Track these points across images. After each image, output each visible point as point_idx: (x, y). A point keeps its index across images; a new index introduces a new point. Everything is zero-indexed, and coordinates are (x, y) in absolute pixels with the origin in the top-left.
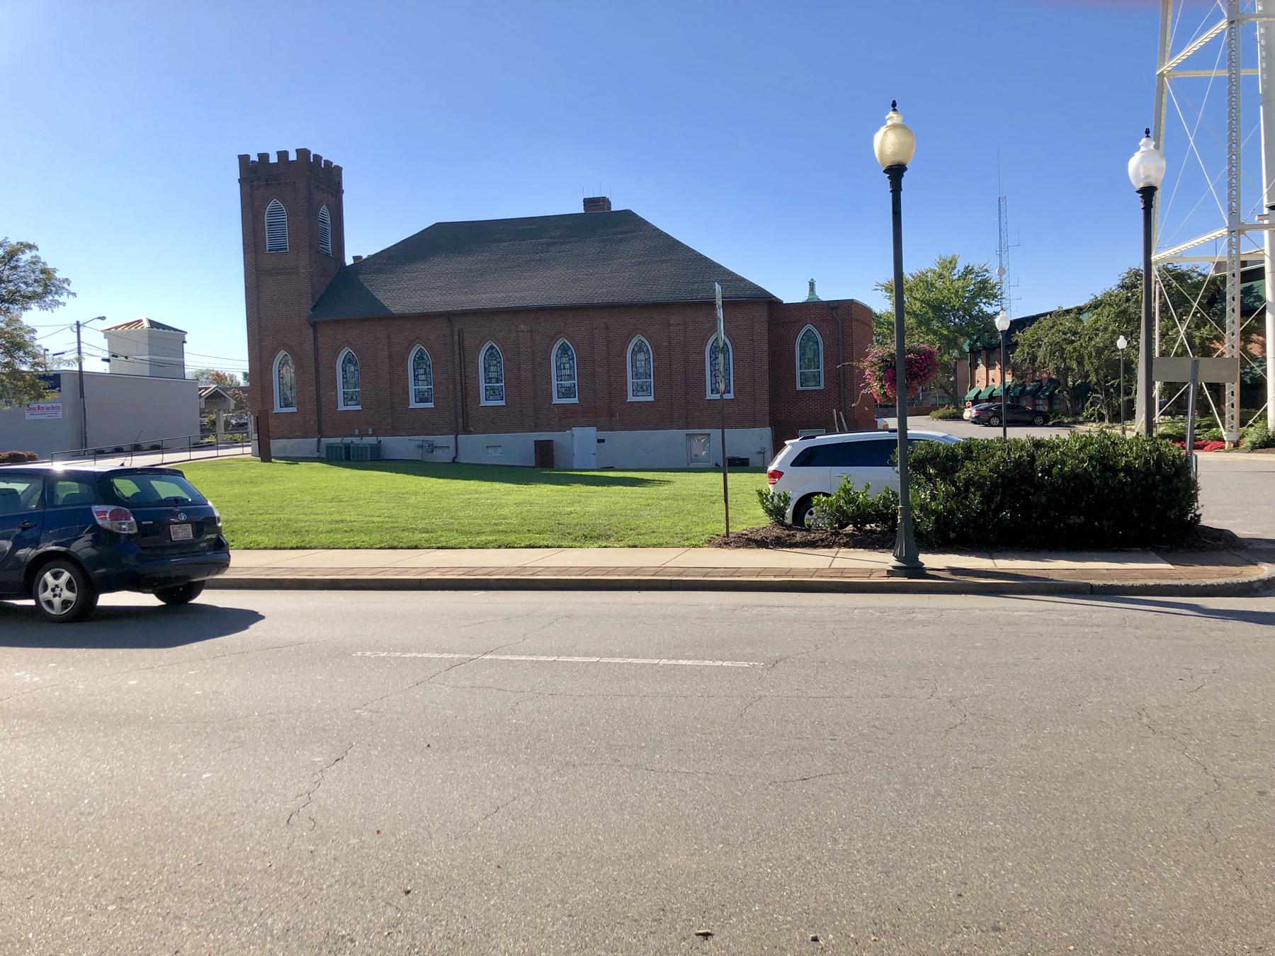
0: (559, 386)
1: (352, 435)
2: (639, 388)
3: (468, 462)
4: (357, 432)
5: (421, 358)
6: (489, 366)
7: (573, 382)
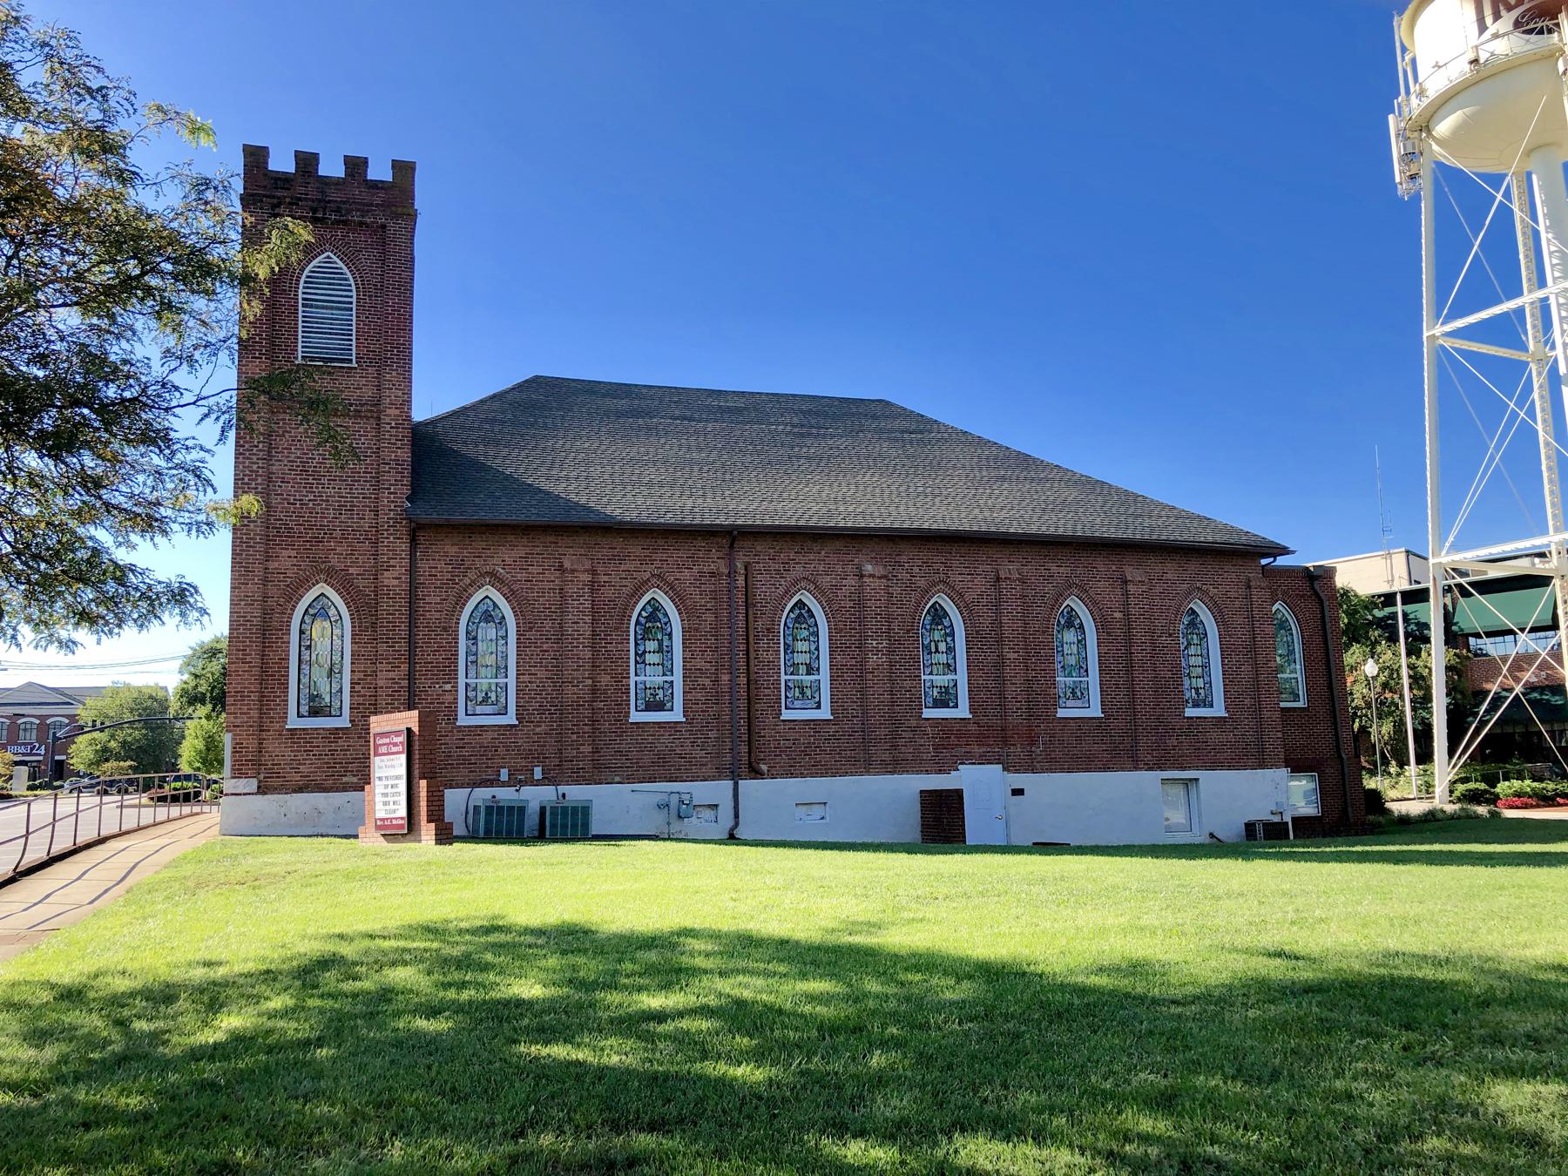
0: (928, 684)
3: (694, 845)
5: (652, 617)
6: (795, 639)
7: (637, 678)
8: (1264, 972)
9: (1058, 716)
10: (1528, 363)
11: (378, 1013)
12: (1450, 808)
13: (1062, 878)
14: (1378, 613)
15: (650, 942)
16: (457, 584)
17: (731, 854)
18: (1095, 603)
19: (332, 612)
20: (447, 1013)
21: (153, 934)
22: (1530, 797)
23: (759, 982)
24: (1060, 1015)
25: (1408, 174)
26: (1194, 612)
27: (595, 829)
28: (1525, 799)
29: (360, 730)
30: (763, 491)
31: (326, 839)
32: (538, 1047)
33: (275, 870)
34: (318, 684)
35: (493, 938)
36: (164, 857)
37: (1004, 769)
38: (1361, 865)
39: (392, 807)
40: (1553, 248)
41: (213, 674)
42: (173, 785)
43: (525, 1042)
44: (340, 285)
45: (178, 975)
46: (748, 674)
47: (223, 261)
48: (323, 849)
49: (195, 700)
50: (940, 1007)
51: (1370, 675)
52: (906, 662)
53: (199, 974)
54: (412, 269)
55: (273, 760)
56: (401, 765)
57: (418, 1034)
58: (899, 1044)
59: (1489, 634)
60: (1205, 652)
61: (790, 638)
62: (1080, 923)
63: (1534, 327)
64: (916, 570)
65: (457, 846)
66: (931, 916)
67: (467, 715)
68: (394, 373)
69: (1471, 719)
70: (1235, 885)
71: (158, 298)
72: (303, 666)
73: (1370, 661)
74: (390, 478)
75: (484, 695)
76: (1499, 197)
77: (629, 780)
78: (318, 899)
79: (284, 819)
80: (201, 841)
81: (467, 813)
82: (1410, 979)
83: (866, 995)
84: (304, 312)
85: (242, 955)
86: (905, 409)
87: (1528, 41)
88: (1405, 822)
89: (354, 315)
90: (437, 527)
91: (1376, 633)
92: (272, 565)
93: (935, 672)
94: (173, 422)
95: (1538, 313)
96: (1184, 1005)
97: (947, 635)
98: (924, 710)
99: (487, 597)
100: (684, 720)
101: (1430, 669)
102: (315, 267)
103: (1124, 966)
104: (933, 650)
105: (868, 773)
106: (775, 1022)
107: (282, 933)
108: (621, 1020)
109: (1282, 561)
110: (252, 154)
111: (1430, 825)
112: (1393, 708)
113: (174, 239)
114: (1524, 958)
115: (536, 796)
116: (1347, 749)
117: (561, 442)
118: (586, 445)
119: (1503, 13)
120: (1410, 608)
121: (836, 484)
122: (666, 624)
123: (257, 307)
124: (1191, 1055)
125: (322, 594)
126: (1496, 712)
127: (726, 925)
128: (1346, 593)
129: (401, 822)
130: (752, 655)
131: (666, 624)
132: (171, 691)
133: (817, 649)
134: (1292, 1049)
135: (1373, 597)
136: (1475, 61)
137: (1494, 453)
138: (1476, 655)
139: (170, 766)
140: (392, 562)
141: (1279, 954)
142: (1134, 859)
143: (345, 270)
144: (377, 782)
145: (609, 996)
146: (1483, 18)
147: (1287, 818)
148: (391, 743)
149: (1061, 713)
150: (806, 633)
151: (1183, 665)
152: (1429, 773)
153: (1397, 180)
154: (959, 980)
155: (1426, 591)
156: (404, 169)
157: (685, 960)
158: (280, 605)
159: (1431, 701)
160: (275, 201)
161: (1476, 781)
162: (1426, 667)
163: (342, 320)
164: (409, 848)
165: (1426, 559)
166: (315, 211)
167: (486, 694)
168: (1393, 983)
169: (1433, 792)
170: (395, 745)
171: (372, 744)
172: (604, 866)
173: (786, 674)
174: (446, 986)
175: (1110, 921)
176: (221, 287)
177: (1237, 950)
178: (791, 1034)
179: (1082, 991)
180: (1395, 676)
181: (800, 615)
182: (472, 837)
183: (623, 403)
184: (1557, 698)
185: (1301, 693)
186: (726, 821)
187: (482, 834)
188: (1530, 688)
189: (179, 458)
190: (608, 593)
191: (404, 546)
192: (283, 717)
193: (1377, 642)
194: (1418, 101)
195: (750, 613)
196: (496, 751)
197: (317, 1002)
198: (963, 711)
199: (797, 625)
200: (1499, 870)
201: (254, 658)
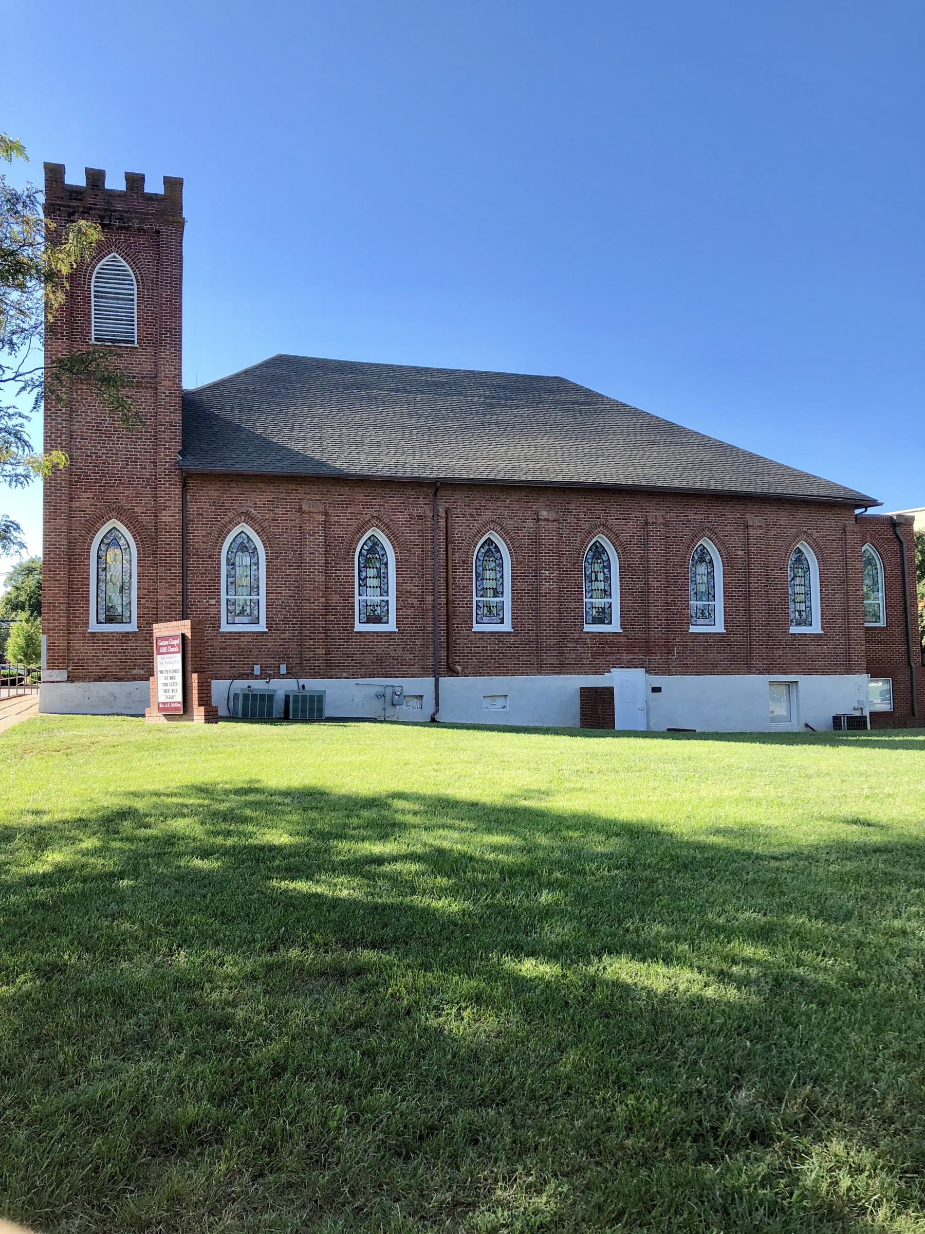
0: (589, 606)
1: (250, 676)
3: (405, 727)
4: (257, 670)
5: (372, 550)
7: (361, 598)
8: (843, 836)
9: (690, 631)
15: (372, 803)
16: (219, 521)
19: (122, 542)
20: (217, 855)
23: (455, 835)
24: (685, 866)
26: (800, 551)
27: (328, 713)
29: (145, 633)
31: (120, 717)
32: (287, 882)
33: (82, 741)
35: (251, 797)
37: (646, 672)
39: (171, 694)
43: (277, 879)
45: (13, 821)
46: (447, 595)
50: (593, 857)
56: (178, 662)
57: (196, 871)
58: (561, 885)
62: (703, 793)
64: (582, 515)
65: (221, 724)
66: (588, 786)
67: (228, 623)
74: (166, 436)
75: (241, 608)
77: (354, 676)
80: (25, 717)
83: (537, 847)
84: (95, 301)
85: (60, 806)
86: (577, 385)
89: (136, 304)
92: (75, 504)
93: (594, 596)
96: (780, 860)
97: (604, 567)
98: (585, 625)
100: (397, 630)
106: (467, 867)
107: (89, 790)
109: (871, 511)
115: (282, 687)
121: (519, 445)
122: (383, 555)
124: (785, 899)
125: (114, 528)
127: (429, 790)
130: (451, 581)
131: (383, 555)
133: (502, 577)
140: (168, 504)
141: (856, 822)
143: (128, 267)
144: (159, 675)
147: (866, 713)
148: (169, 645)
149: (693, 629)
151: (790, 592)
156: (174, 185)
157: (400, 817)
160: (71, 210)
170: (173, 646)
171: (155, 645)
174: (215, 834)
175: (726, 793)
179: (702, 847)
181: (489, 550)
182: (232, 718)
185: (881, 615)
186: (429, 709)
187: (240, 715)
190: (338, 530)
191: (178, 491)
196: (251, 651)
198: (615, 627)
199: (486, 558)
201: (62, 575)
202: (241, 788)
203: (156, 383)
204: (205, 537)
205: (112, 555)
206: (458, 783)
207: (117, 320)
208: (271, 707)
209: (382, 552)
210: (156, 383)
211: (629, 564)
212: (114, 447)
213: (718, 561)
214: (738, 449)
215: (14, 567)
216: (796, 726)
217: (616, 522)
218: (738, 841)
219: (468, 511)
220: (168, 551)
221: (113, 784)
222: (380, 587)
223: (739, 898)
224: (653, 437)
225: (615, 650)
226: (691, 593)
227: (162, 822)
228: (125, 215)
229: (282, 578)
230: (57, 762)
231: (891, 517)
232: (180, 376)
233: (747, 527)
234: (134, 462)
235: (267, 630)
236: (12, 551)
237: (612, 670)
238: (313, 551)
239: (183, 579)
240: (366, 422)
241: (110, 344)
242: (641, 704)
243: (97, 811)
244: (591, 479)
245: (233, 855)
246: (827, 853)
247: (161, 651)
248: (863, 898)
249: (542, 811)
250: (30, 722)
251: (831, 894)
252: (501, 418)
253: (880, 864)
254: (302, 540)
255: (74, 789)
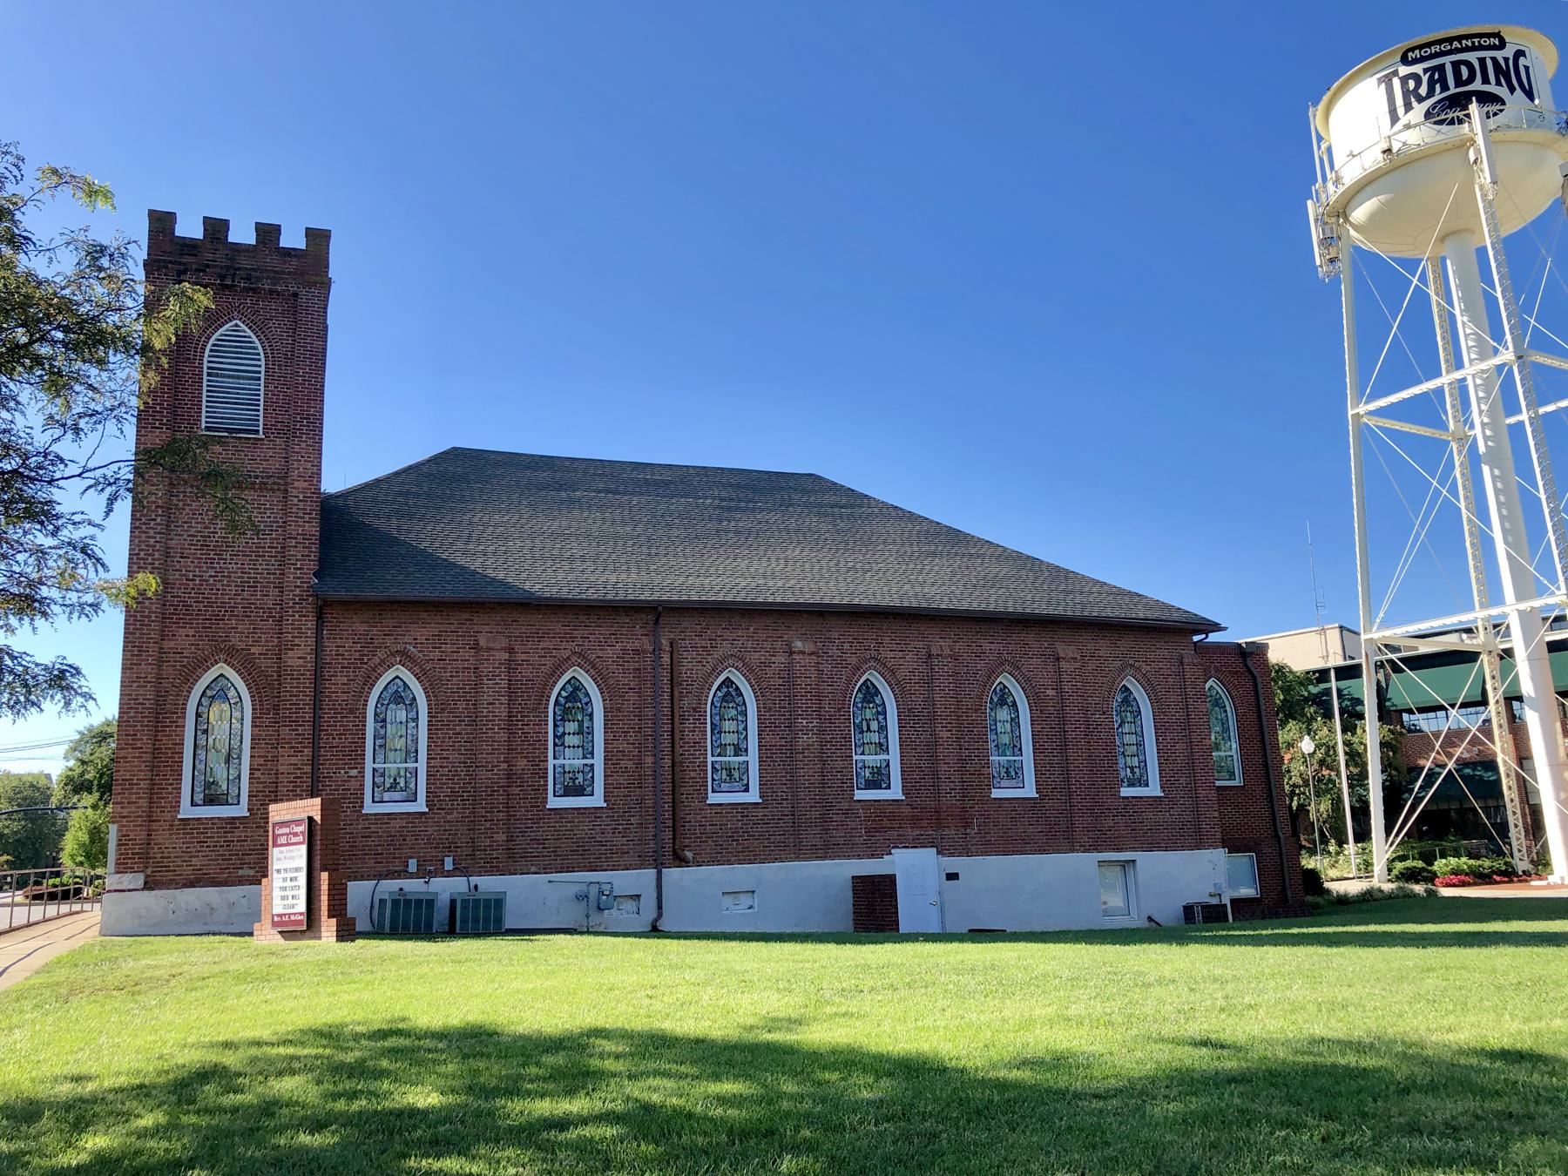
0: (860, 765)
1: (403, 873)
2: (1003, 774)
4: (413, 865)
5: (572, 697)
7: (556, 762)
8: (1188, 1062)
9: (992, 796)
10: (1449, 442)
11: (258, 1130)
12: (1388, 887)
13: (993, 967)
14: (1314, 690)
15: (556, 1044)
16: (366, 663)
17: (651, 948)
18: (1028, 680)
19: (232, 693)
20: (334, 1127)
21: (18, 1046)
22: (1467, 874)
23: (670, 1084)
24: (978, 1112)
25: (1328, 257)
26: (1127, 689)
27: (509, 923)
28: (1462, 877)
29: (258, 820)
30: (690, 566)
31: (218, 938)
32: (430, 1161)
33: (158, 973)
34: (215, 769)
35: (391, 1042)
36: (37, 961)
38: (1295, 948)
39: (290, 901)
40: (1468, 331)
41: (102, 760)
42: (51, 882)
43: (416, 1156)
44: (248, 354)
45: (42, 1092)
46: (673, 756)
47: (118, 328)
48: (214, 948)
49: (81, 789)
50: (856, 1107)
51: (1306, 752)
52: (836, 746)
53: (65, 1090)
54: (324, 338)
55: (163, 853)
56: (301, 856)
57: (305, 1150)
58: (811, 1147)
59: (1422, 710)
60: (1139, 729)
61: (718, 718)
62: (1007, 1013)
63: (1453, 406)
64: (847, 646)
65: (360, 942)
66: (855, 1010)
67: (373, 802)
68: (303, 445)
69: (1406, 795)
70: (1167, 971)
71: (47, 366)
72: (199, 752)
73: (1307, 738)
74: (295, 553)
75: (392, 781)
76: (1415, 281)
77: (546, 870)
78: (204, 1004)
79: (172, 917)
80: (77, 943)
81: (372, 907)
82: (1334, 1066)
83: (781, 1096)
84: (208, 381)
85: (114, 1068)
86: (836, 484)
87: (1438, 131)
88: (1343, 901)
89: (262, 385)
90: (345, 604)
91: (1312, 710)
92: (168, 645)
93: (867, 752)
94: (57, 495)
95: (1456, 392)
96: (1105, 1098)
97: (878, 713)
98: (856, 792)
99: (397, 677)
100: (605, 805)
101: (1365, 745)
102: (221, 335)
103: (1048, 1059)
104: (865, 729)
105: (798, 858)
106: (683, 1127)
107: (160, 1044)
108: (521, 1129)
109: (1214, 637)
110: (159, 220)
111: (1368, 905)
112: (1331, 786)
113: (67, 306)
114: (1447, 1043)
115: (447, 887)
116: (1284, 829)
117: (479, 516)
118: (507, 518)
119: (1415, 104)
120: (1344, 684)
121: (765, 558)
122: (586, 704)
123: (153, 378)
124: (1109, 1152)
125: (222, 675)
126: (1431, 787)
127: (639, 1024)
128: (1281, 670)
129: (300, 918)
130: (677, 737)
131: (586, 704)
132: (54, 778)
133: (746, 729)
134: (1211, 1143)
135: (1308, 673)
136: (1388, 151)
137: (1419, 531)
138: (1409, 731)
139: (51, 860)
140: (297, 641)
141: (1205, 1043)
142: (1068, 946)
143: (254, 338)
144: (275, 875)
145: (509, 1103)
146: (1396, 109)
147: (1226, 901)
148: (290, 833)
149: (996, 793)
150: (734, 712)
151: (1118, 743)
152: (1367, 851)
153: (1318, 263)
154: (878, 1078)
155: (1359, 666)
156: (319, 238)
157: (595, 1063)
158: (176, 687)
159: (1367, 778)
160: (182, 268)
161: (1414, 859)
162: (1361, 743)
163: (250, 389)
164: (308, 947)
165: (1357, 634)
166: (223, 278)
167: (395, 779)
168: (1317, 1070)
169: (1373, 871)
170: (295, 834)
171: (270, 833)
172: (515, 962)
173: (713, 756)
174: (336, 1096)
175: (1037, 1012)
176: (115, 355)
177: (1163, 1040)
178: (700, 1139)
179: (1002, 1086)
180: (1331, 753)
181: (728, 694)
182: (377, 933)
183: (544, 476)
184: (1490, 774)
185: (1236, 771)
186: (649, 913)
187: (387, 929)
188: (1462, 764)
189: (65, 534)
190: (526, 671)
191: (311, 624)
192: (175, 807)
193: (1313, 719)
194: (1334, 188)
195: (676, 693)
196: (404, 840)
197: (193, 1119)
198: (895, 792)
199: (724, 704)
200: (1431, 951)
201: (145, 741)
202: (379, 1030)
203: (287, 484)
204: (344, 684)
205: (214, 712)
206: (679, 1014)
207: (226, 403)
208: (430, 917)
209: (585, 700)
210: (287, 484)
211: (909, 709)
212: (226, 568)
213: (1023, 703)
214: (1042, 561)
215: (79, 733)
216: (1136, 921)
217: (892, 654)
218: (1049, 1075)
219: (700, 643)
220: (294, 704)
221: (195, 1031)
222: (583, 747)
223: (1048, 1153)
224: (933, 548)
225: (896, 824)
226: (991, 745)
227: (261, 1083)
228: (253, 273)
229: (450, 738)
230: (117, 1005)
231: (1239, 645)
232: (318, 474)
233: (1058, 659)
234: (252, 587)
235: (427, 810)
236: (73, 706)
237: (893, 851)
238: (493, 700)
239: (313, 743)
240: (566, 532)
241: (226, 434)
242: (934, 898)
243: (167, 1072)
244: (857, 599)
245: (357, 1125)
246: (1167, 1087)
247: (279, 842)
248: (1213, 1146)
249: (791, 1047)
250: (84, 950)
251: (1171, 1143)
252: (741, 524)
253: (1235, 1098)
254: (477, 686)
255: (139, 1042)
